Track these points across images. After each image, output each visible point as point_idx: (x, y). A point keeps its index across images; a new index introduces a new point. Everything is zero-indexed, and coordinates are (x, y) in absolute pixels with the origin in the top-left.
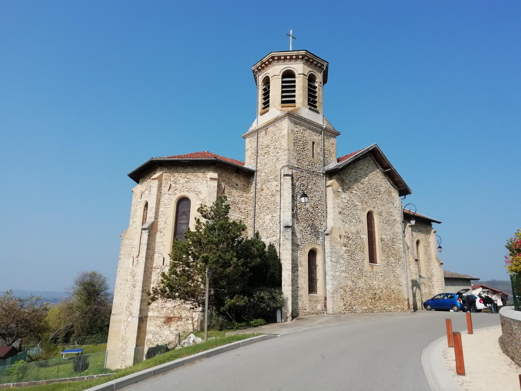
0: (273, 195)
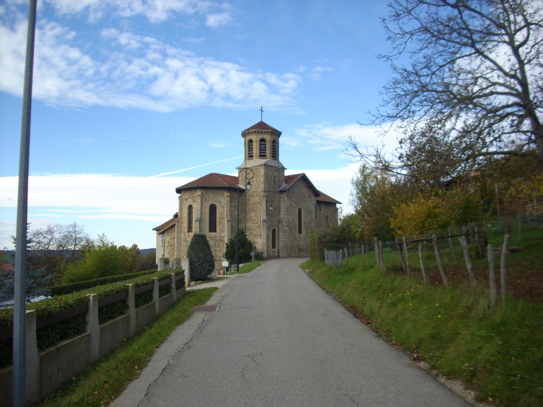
0: (256, 204)
